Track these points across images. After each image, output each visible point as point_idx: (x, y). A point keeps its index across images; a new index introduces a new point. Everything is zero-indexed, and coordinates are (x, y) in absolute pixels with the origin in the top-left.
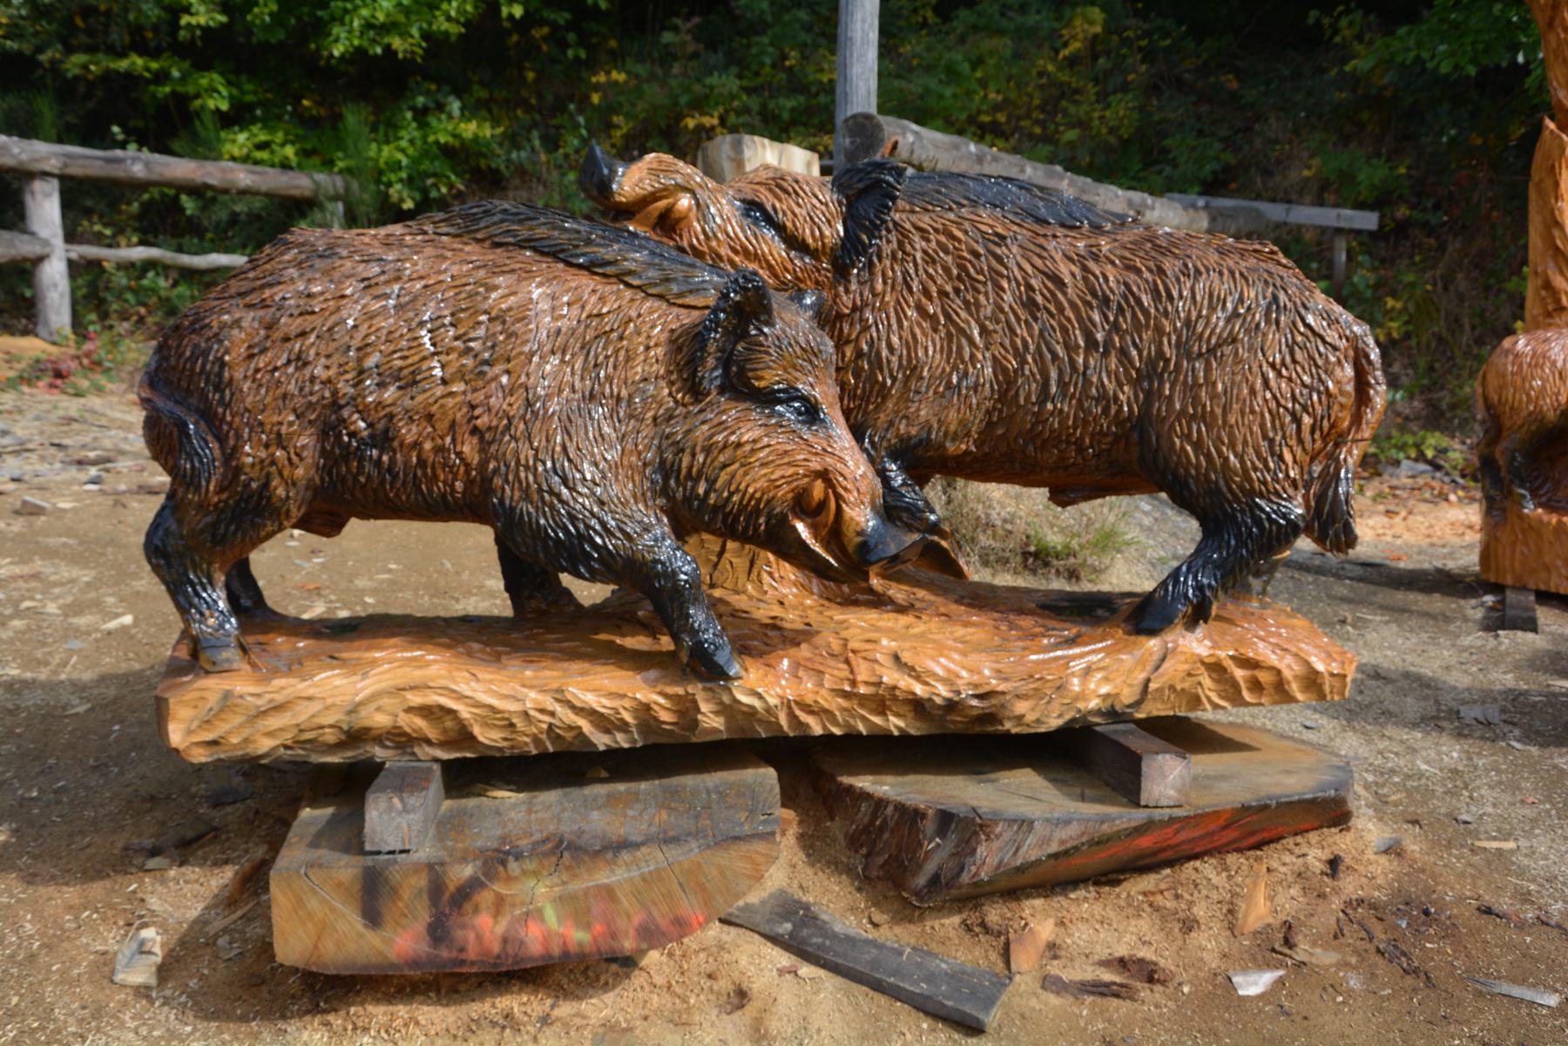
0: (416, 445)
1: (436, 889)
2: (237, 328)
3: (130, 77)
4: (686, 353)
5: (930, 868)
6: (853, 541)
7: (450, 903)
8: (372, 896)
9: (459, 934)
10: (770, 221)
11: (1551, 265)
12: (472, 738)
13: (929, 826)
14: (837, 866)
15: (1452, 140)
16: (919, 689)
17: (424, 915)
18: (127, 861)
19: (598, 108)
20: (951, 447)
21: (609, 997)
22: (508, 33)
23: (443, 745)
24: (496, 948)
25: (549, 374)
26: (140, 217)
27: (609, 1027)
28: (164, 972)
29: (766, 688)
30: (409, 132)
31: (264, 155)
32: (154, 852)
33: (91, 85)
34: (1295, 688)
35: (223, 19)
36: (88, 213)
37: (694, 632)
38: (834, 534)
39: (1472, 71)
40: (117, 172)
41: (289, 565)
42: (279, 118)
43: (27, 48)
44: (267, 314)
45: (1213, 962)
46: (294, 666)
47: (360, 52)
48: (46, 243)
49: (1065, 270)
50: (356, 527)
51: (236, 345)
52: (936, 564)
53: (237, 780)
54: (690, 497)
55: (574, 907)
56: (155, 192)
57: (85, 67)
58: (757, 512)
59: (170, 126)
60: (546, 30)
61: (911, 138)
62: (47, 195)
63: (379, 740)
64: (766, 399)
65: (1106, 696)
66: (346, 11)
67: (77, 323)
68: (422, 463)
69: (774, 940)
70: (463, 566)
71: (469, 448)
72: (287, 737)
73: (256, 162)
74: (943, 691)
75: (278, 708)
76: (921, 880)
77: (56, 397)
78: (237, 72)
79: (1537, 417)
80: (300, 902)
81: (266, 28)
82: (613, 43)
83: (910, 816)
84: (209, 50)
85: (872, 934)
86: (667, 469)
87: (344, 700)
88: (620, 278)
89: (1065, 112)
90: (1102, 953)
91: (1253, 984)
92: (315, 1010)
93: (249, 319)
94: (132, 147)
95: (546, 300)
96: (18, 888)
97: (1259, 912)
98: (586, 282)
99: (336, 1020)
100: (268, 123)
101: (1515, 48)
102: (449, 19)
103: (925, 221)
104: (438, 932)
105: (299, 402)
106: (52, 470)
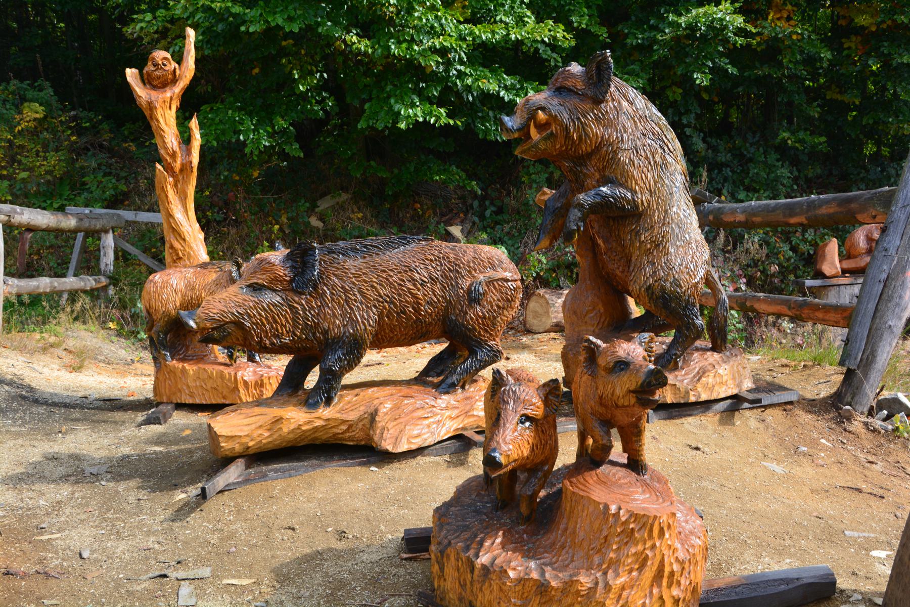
11: (172, 236)
15: (226, 177)
79: (167, 314)
89: (20, 162)
101: (239, 132)
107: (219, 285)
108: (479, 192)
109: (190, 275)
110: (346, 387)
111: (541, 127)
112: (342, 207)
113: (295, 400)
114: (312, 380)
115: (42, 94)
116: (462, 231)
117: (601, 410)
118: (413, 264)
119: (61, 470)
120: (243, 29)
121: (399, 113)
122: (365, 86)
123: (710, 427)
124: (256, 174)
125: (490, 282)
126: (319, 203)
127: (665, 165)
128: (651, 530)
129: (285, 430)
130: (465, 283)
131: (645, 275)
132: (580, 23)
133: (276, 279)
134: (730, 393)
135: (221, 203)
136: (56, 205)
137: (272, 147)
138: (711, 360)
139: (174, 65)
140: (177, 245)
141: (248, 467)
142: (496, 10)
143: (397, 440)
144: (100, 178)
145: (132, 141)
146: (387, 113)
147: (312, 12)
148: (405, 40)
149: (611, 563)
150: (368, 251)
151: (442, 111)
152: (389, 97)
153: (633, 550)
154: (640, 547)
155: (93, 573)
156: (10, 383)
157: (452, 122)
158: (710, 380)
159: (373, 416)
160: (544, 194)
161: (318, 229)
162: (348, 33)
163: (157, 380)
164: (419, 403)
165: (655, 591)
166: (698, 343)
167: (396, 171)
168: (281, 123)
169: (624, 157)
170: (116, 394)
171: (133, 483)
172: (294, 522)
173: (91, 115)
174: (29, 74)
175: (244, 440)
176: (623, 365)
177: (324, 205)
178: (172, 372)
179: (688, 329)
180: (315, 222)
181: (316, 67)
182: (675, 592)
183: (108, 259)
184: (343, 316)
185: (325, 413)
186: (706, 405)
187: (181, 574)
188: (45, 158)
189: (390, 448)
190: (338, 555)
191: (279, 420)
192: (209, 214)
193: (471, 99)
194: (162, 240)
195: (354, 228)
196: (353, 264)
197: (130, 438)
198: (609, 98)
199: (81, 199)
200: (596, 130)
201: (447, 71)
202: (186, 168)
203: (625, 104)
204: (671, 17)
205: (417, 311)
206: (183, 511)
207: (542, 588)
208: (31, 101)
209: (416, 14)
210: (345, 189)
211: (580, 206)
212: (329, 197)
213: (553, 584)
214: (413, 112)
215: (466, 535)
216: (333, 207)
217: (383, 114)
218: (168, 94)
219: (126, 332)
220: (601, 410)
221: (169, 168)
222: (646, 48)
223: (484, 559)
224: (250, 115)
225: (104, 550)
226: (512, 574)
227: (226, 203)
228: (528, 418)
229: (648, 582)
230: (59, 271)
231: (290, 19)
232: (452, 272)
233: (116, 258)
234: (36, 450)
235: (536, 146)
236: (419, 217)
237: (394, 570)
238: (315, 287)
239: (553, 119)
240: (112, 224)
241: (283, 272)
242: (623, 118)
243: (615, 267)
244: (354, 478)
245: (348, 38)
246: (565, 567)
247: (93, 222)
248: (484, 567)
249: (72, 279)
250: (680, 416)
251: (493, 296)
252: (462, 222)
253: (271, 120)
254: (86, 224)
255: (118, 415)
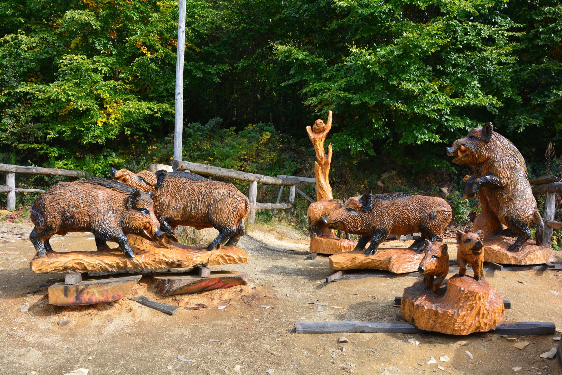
0: (78, 218)
1: (77, 290)
2: (48, 199)
3: (34, 149)
4: (126, 202)
5: (166, 289)
6: (154, 233)
7: (79, 292)
8: (66, 292)
9: (81, 298)
10: (144, 180)
12: (86, 268)
13: (167, 282)
14: (152, 292)
15: (342, 163)
16: (167, 260)
17: (75, 295)
18: (23, 295)
19: (149, 155)
20: (175, 219)
21: (108, 311)
22: (128, 137)
23: (81, 270)
24: (87, 301)
25: (102, 206)
26: (34, 182)
27: (108, 315)
28: (29, 310)
29: (139, 260)
30: (102, 161)
31: (66, 167)
32: (29, 293)
33: (24, 151)
34: (237, 261)
35: (57, 135)
36: (21, 181)
37: (126, 249)
38: (151, 233)
39: (338, 150)
40: (29, 171)
41: (55, 240)
42: (70, 158)
43: (9, 143)
44: (53, 196)
45: (215, 304)
46: (56, 257)
47: (90, 143)
48: (11, 188)
49: (195, 188)
50: (69, 234)
51: (47, 201)
52: (171, 239)
53: (45, 283)
54: (126, 227)
55: (101, 293)
56: (38, 176)
57: (23, 147)
58: (137, 229)
59: (43, 160)
60: (138, 136)
61: (186, 165)
62: (12, 177)
63: (70, 269)
64: (140, 210)
65: (201, 261)
66: (88, 133)
67: (16, 206)
68: (79, 221)
69: (138, 302)
70: (88, 240)
71: (87, 218)
72: (53, 269)
73: (64, 169)
74: (171, 260)
75: (52, 263)
76: (165, 292)
77: (11, 223)
78: (60, 147)
79: (316, 219)
80: (53, 292)
81: (67, 137)
82: (155, 139)
83: (164, 281)
84: (53, 143)
85: (156, 301)
86: (122, 222)
87: (64, 262)
88: (115, 190)
89: (260, 156)
90: (196, 303)
91: (221, 308)
92: (56, 314)
93: (50, 197)
94: (33, 165)
95: (102, 193)
96: (3, 300)
97: (226, 297)
98: (109, 190)
99: (59, 315)
100: (67, 159)
101: (348, 145)
102: (112, 135)
103: (172, 180)
104: (77, 298)
105: (58, 211)
106: (10, 236)
107: (336, 208)
108: (457, 172)
109: (326, 204)
110: (381, 249)
111: (462, 152)
112: (392, 177)
113: (361, 252)
114: (368, 245)
115: (270, 128)
116: (448, 190)
117: (463, 256)
118: (410, 204)
119: (279, 271)
120: (352, 103)
121: (417, 137)
122: (404, 125)
123: (530, 275)
124: (355, 162)
125: (438, 212)
126: (382, 175)
127: (515, 168)
128: (475, 297)
129: (357, 262)
130: (428, 212)
131: (504, 212)
132: (507, 95)
133: (356, 207)
134: (541, 263)
135: (339, 175)
136: (273, 174)
137: (362, 150)
138: (534, 248)
139: (324, 125)
140: (321, 193)
141: (343, 275)
142: (465, 91)
143: (398, 269)
144: (290, 163)
145: (304, 146)
146: (413, 137)
147: (381, 95)
148: (421, 106)
149: (460, 307)
150: (391, 198)
151: (437, 136)
152: (414, 130)
153: (468, 303)
154: (471, 303)
155: (290, 300)
156: (259, 242)
157: (441, 141)
158: (532, 256)
159: (390, 259)
160: (467, 177)
161: (381, 187)
162: (397, 102)
163: (311, 243)
164: (408, 256)
165: (477, 319)
166: (529, 241)
167: (417, 162)
168: (366, 141)
169: (497, 165)
170: (295, 249)
171: (302, 277)
172: (357, 293)
173: (288, 136)
174: (266, 120)
175: (342, 264)
176: (469, 240)
177: (385, 176)
178: (317, 241)
179: (524, 235)
180: (380, 184)
181: (383, 116)
182: (485, 321)
183: (292, 197)
184: (381, 222)
185: (372, 257)
186: (530, 267)
187: (318, 303)
188: (270, 154)
189: (395, 272)
190: (372, 303)
191: (355, 258)
192: (334, 179)
193: (452, 130)
194: (314, 189)
195: (397, 187)
196: (385, 202)
197: (302, 263)
198: (491, 140)
199: (282, 172)
200: (486, 153)
201: (441, 118)
202: (326, 163)
203: (498, 143)
204: (554, 91)
205: (409, 221)
206: (319, 287)
207: (436, 313)
208: (266, 131)
209: (426, 95)
210: (394, 169)
211: (477, 183)
212: (387, 173)
213: (440, 312)
214: (424, 137)
215: (413, 296)
216: (388, 177)
217: (410, 137)
218: (321, 136)
219: (299, 226)
220: (463, 256)
221: (320, 163)
222: (543, 105)
223: (418, 302)
224: (353, 137)
225: (294, 295)
226: (425, 307)
227: (342, 174)
228: (435, 257)
229: (474, 315)
230: (273, 201)
231: (372, 99)
232: (424, 207)
233: (296, 196)
234: (270, 264)
235: (460, 159)
236: (428, 183)
237: (390, 309)
238: (371, 210)
239: (467, 149)
240: (295, 182)
241: (359, 204)
242: (497, 149)
243: (493, 208)
244: (381, 281)
245: (397, 105)
246: (444, 307)
247: (288, 181)
248: (417, 305)
249: (279, 204)
250: (518, 270)
251: (440, 217)
252: (448, 186)
253: (362, 139)
254: (285, 182)
255: (297, 256)
